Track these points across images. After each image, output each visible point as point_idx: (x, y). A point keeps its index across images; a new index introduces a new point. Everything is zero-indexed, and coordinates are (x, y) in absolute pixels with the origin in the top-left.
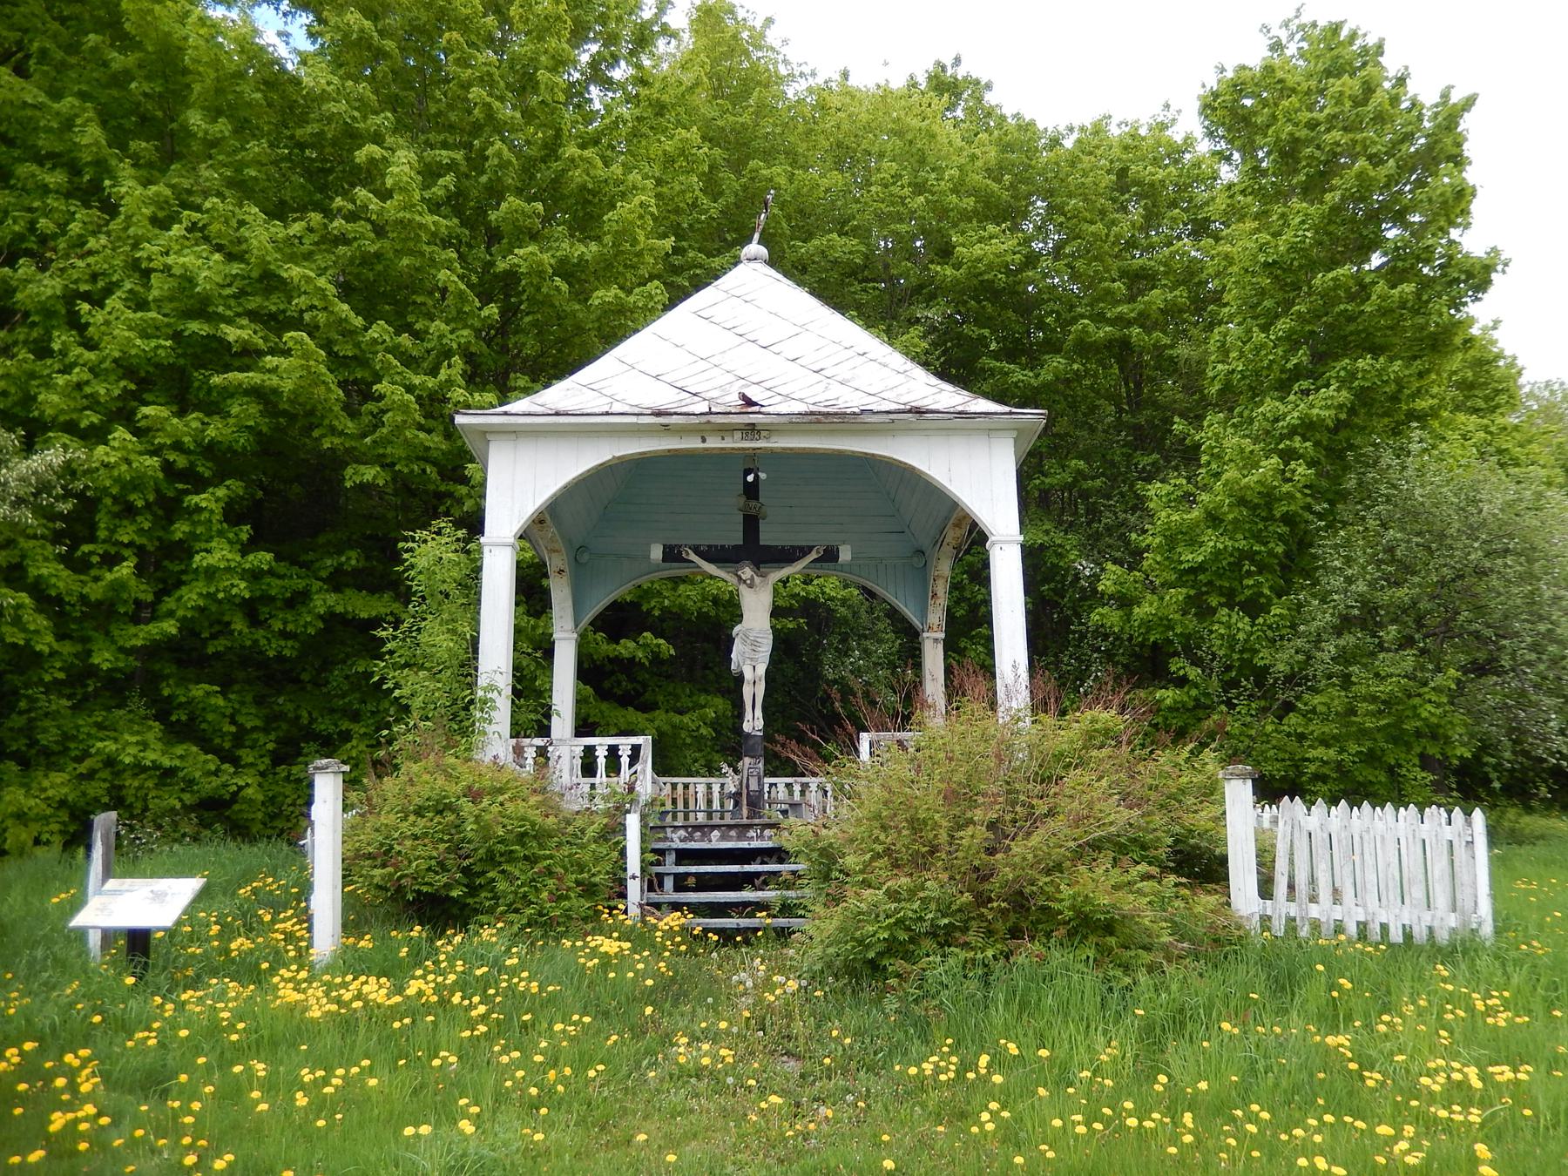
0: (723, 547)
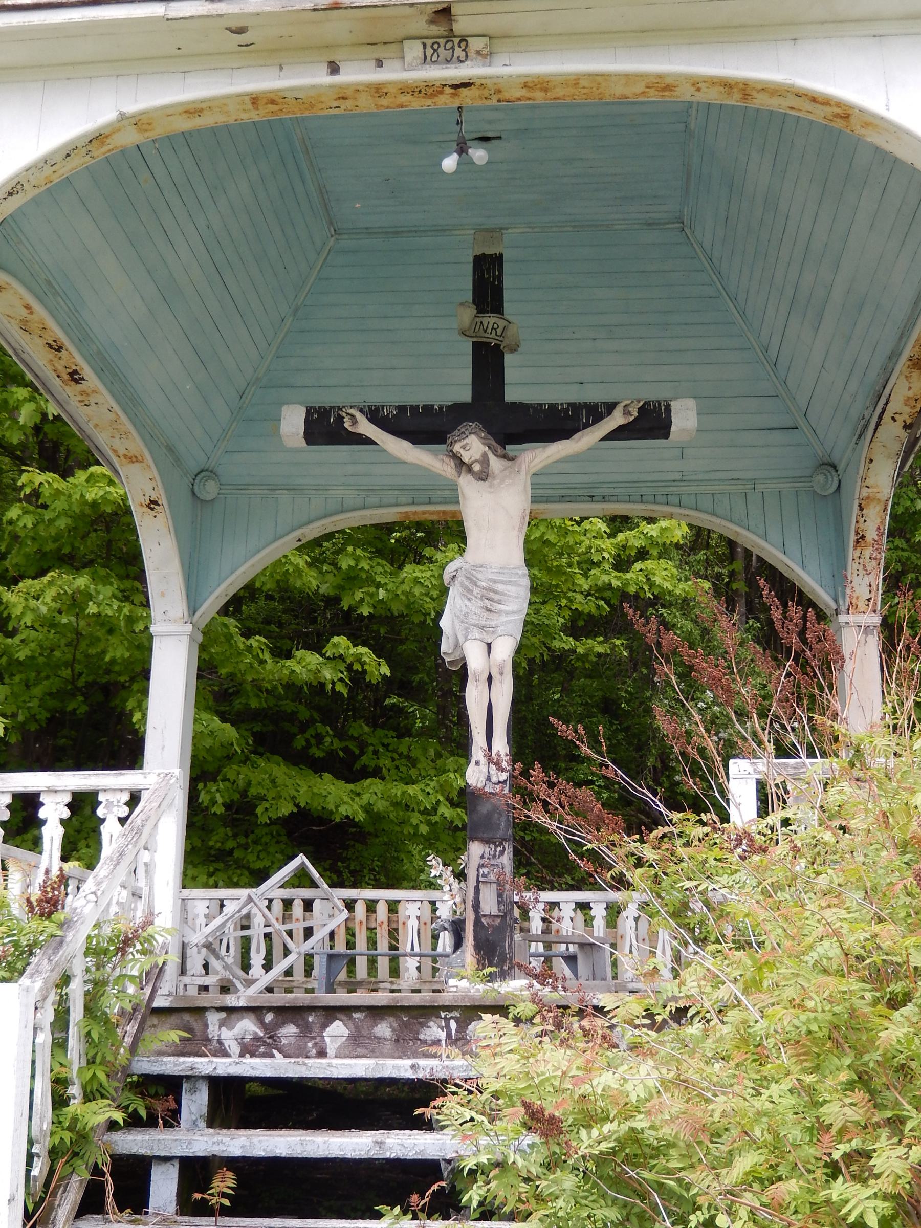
0: (428, 408)
